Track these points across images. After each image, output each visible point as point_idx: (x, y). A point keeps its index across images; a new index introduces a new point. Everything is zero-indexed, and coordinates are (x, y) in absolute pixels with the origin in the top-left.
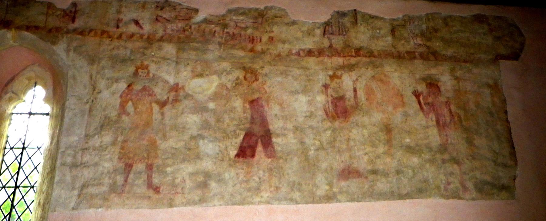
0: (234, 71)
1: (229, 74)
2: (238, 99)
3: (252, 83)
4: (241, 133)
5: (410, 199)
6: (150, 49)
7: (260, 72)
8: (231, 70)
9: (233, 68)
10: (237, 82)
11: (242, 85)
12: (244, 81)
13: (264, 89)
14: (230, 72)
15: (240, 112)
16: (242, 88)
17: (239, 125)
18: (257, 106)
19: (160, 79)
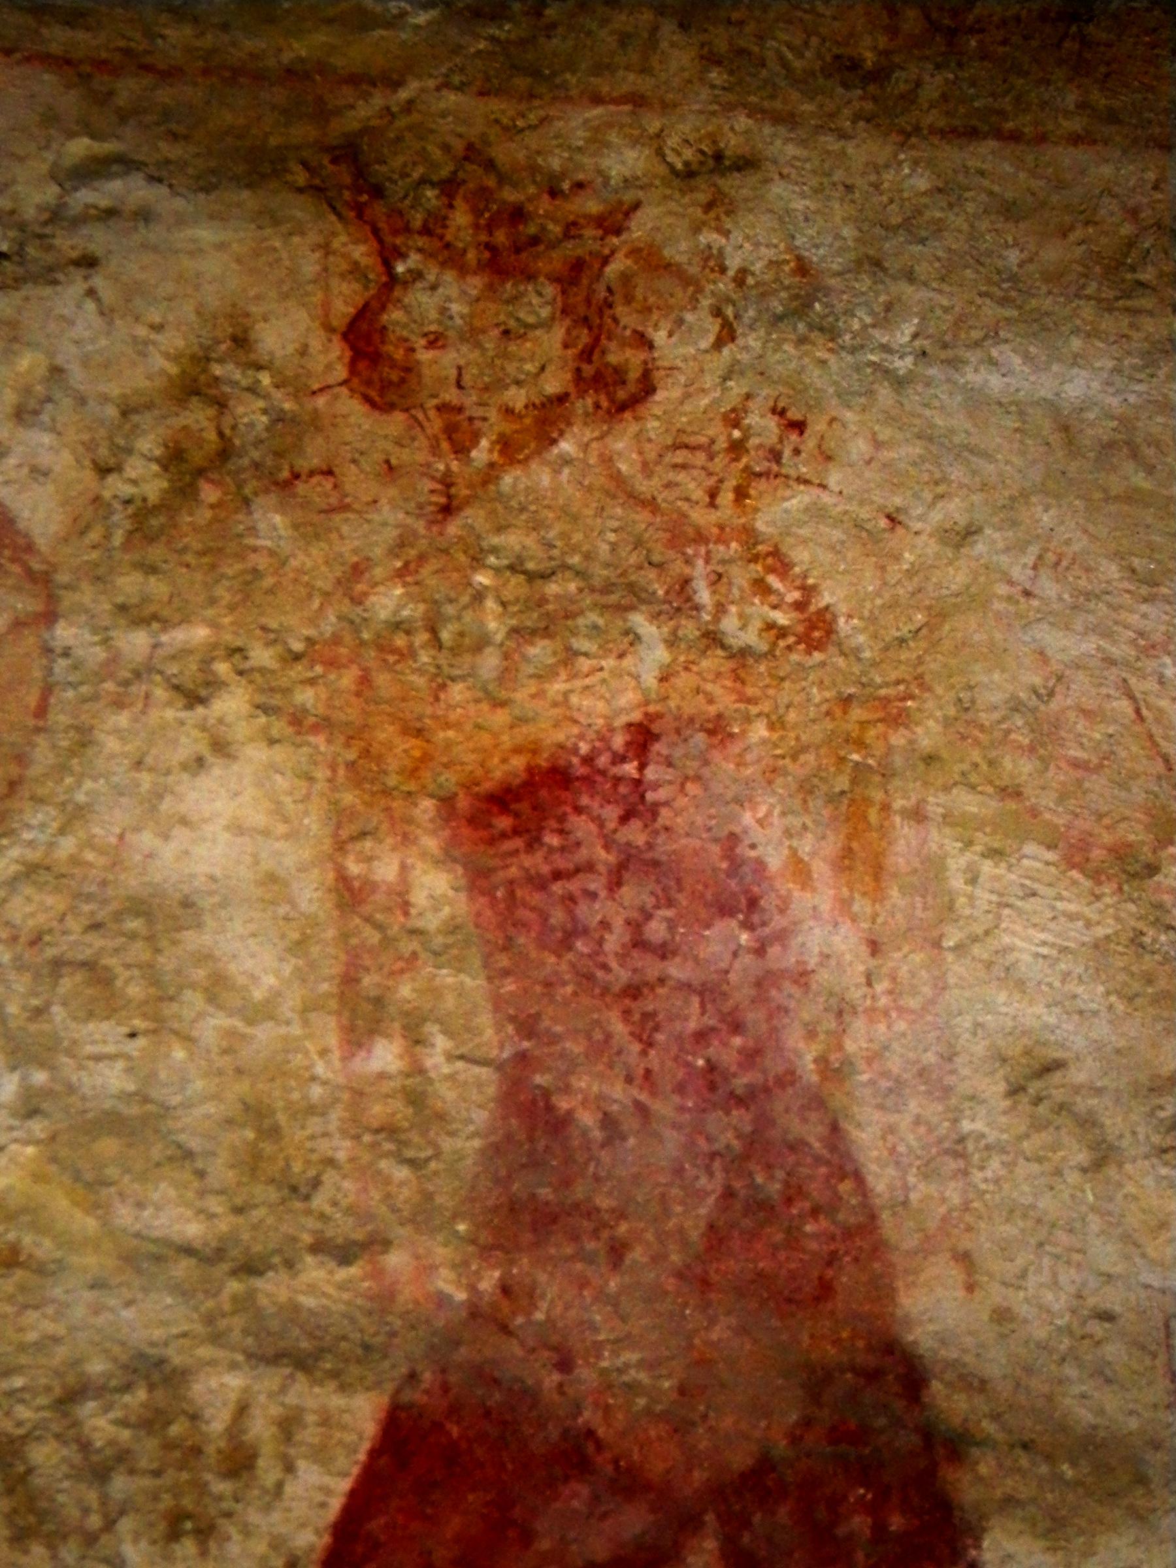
0: (144, 215)
1: (49, 276)
2: (221, 747)
3: (508, 448)
4: (288, 1425)
5: (373, 1454)
6: (544, 764)
7: (679, 251)
8: (85, 197)
9: (125, 164)
10: (198, 417)
11: (315, 490)
12: (352, 407)
13: (780, 563)
14: (68, 244)
15: (265, 1012)
16: (308, 533)
17: (251, 1268)
18: (633, 894)
19: (736, 1234)
